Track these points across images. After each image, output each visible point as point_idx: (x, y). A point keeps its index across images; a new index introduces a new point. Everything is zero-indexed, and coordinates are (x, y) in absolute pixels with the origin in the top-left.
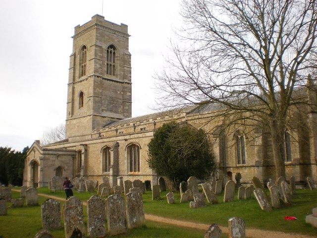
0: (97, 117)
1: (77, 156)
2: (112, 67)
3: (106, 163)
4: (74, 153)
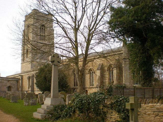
4: (17, 80)
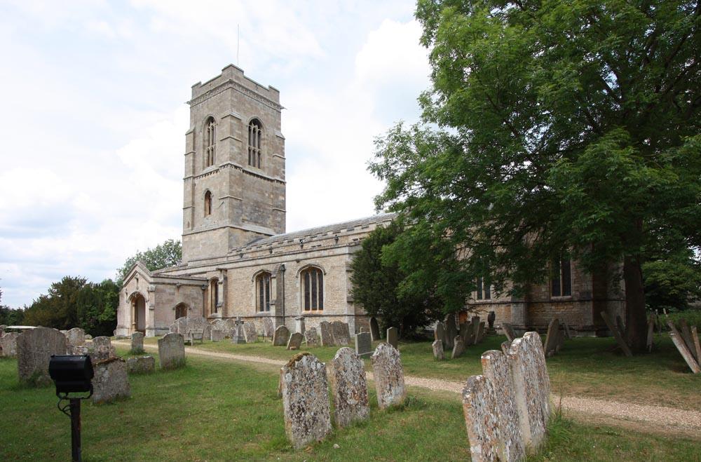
0: (235, 230)
1: (210, 288)
2: (256, 154)
3: (262, 297)
4: (205, 283)
